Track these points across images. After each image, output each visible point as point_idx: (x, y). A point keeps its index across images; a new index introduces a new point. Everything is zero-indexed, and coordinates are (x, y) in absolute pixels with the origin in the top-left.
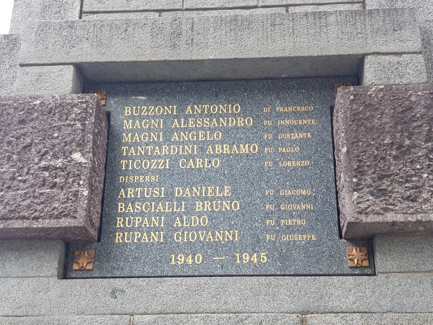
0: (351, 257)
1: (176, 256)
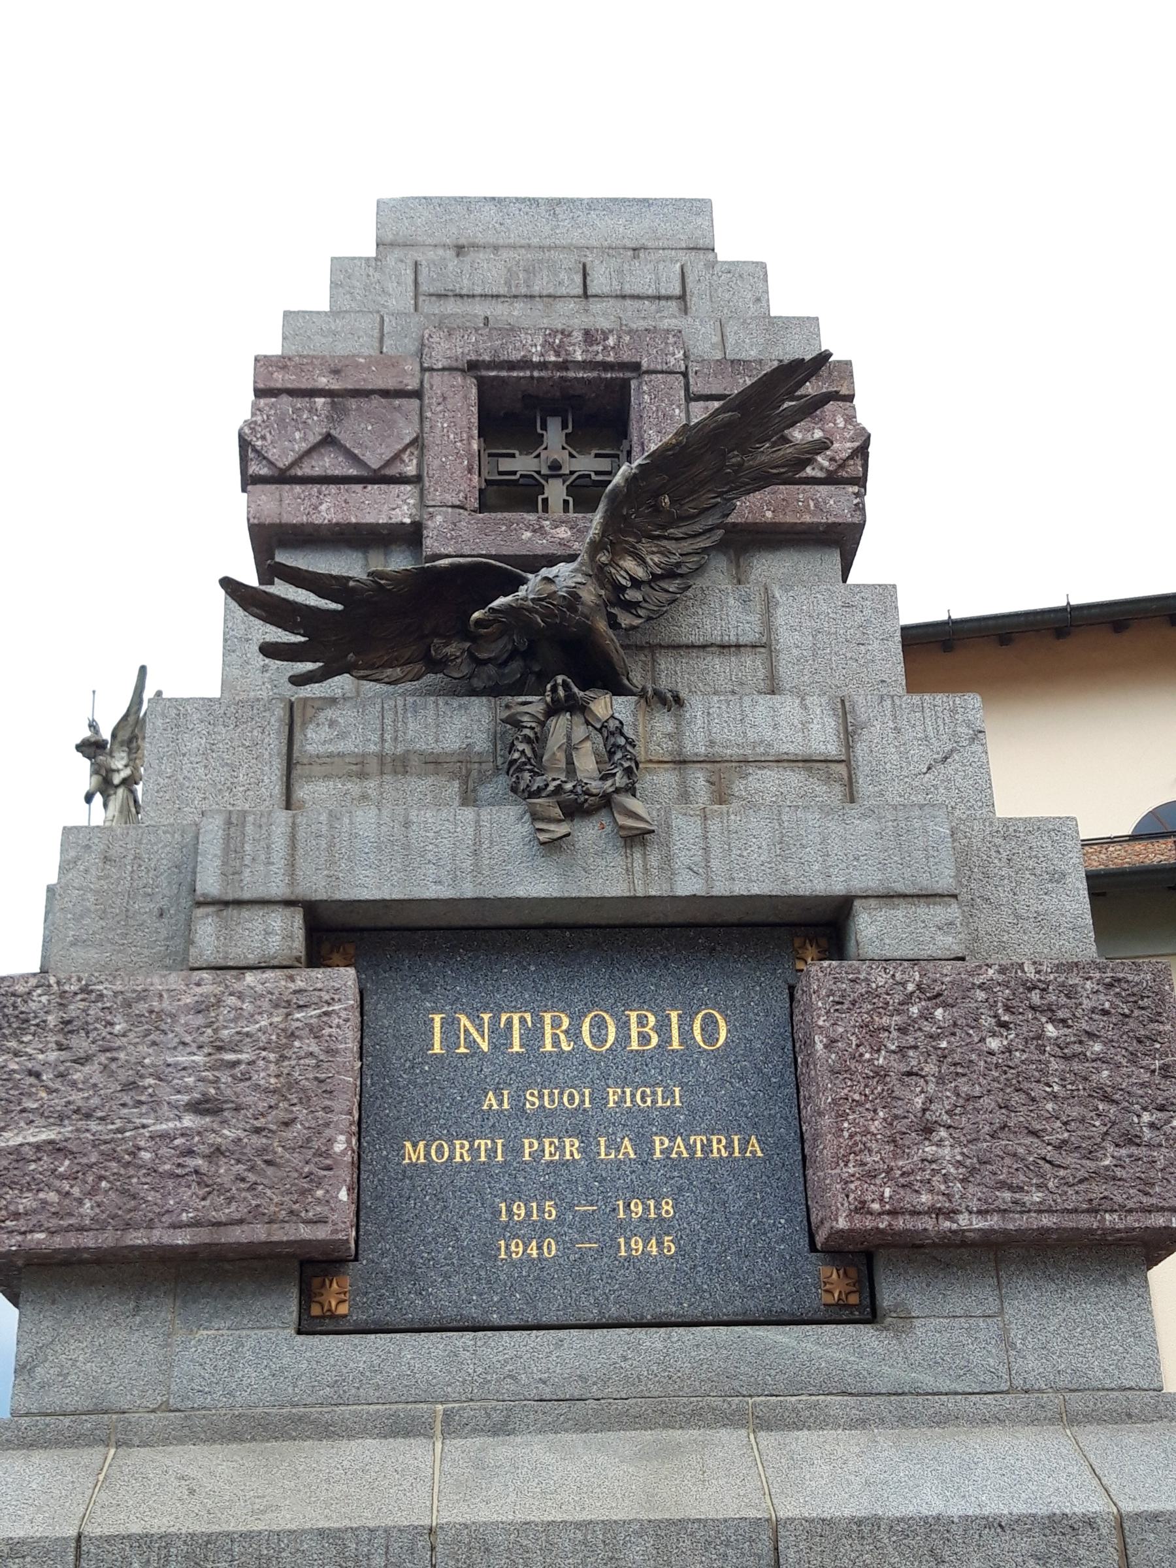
0: (828, 1286)
1: (510, 1231)
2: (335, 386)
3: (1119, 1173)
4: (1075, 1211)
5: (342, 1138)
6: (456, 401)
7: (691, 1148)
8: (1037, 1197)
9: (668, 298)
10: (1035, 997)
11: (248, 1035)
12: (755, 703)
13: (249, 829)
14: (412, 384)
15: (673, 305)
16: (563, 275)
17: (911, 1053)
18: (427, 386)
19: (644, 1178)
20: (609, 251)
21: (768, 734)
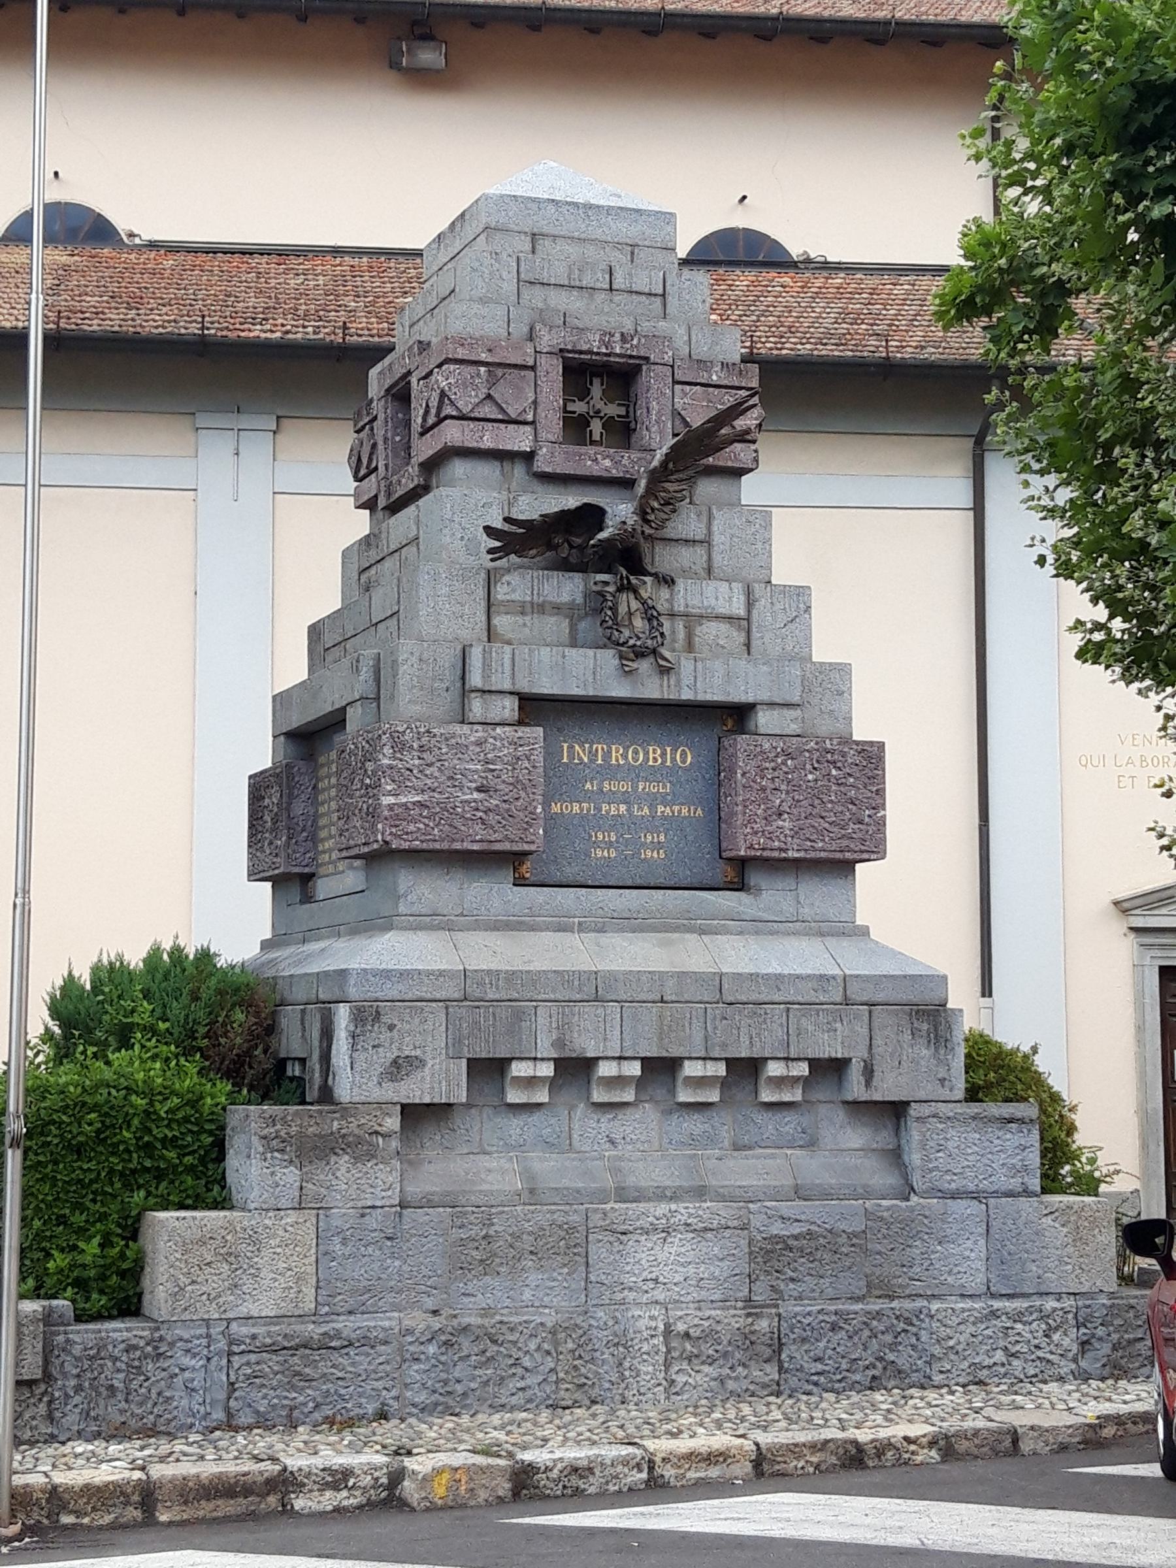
2: (490, 360)
8: (820, 845)
10: (829, 756)
14: (531, 363)
21: (713, 602)
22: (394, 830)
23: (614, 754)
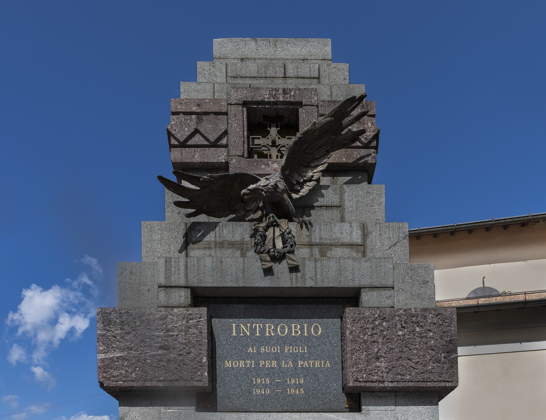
3: (433, 371)
4: (419, 381)
5: (205, 358)
6: (240, 116)
7: (309, 364)
8: (408, 377)
9: (314, 78)
10: (414, 319)
11: (176, 327)
12: (335, 225)
13: (173, 263)
15: (316, 81)
16: (277, 69)
17: (375, 336)
18: (229, 110)
19: (295, 372)
20: (293, 60)
21: (339, 236)
22: (105, 375)
23: (267, 329)
